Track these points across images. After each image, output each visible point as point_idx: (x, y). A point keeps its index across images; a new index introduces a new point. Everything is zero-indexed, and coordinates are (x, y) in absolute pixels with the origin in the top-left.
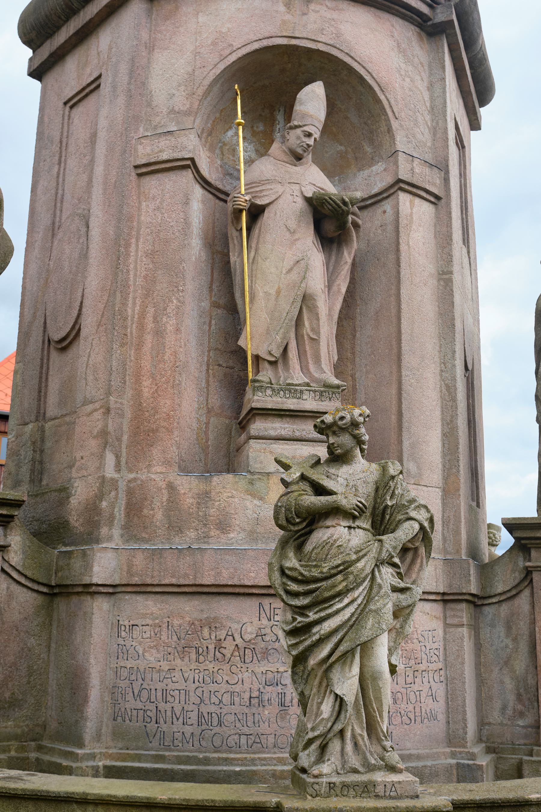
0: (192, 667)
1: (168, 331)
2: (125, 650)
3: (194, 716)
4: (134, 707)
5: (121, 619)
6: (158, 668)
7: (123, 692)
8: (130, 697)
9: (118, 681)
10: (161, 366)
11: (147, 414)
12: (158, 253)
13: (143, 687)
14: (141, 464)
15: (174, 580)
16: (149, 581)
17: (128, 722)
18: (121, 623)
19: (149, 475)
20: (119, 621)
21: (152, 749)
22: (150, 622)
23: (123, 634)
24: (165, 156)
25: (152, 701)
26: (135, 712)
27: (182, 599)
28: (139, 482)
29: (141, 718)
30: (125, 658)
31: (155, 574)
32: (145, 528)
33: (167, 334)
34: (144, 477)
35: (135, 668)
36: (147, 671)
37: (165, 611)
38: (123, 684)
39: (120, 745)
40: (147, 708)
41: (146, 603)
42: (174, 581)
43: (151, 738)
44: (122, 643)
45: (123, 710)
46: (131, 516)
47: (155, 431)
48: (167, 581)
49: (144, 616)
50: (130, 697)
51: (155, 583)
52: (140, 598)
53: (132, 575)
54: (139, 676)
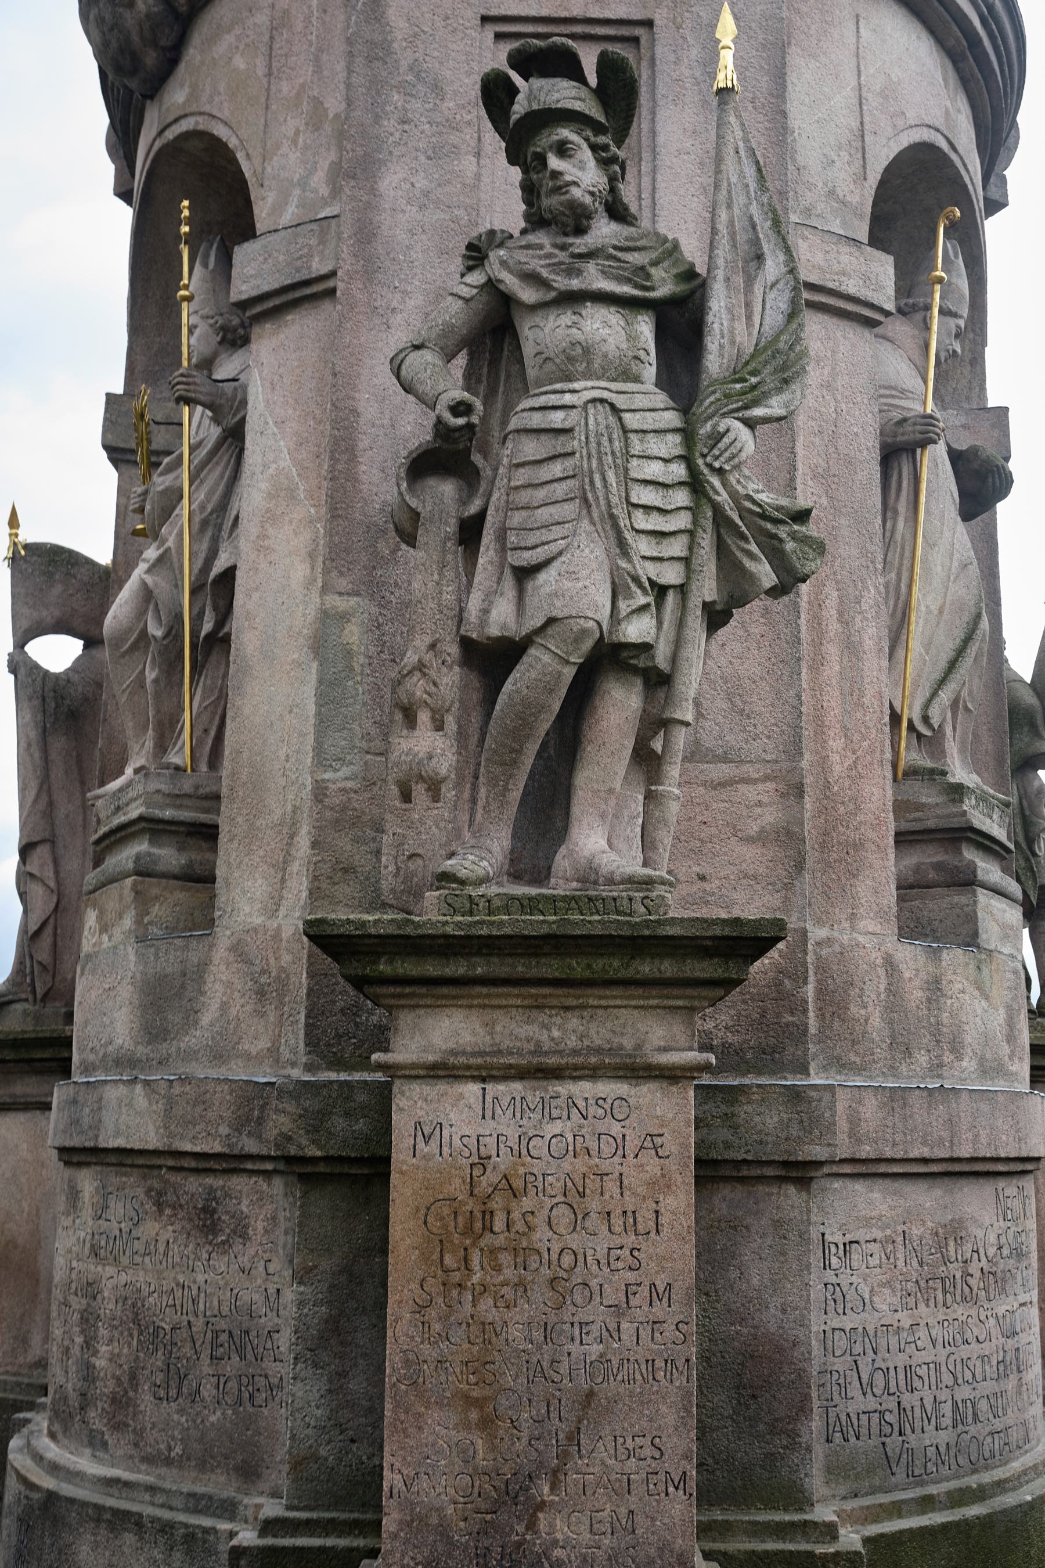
0: (941, 1317)
1: (866, 648)
2: (838, 1295)
3: (947, 1409)
4: (863, 1408)
5: (827, 1232)
6: (896, 1324)
7: (842, 1381)
8: (854, 1390)
9: (831, 1359)
10: (859, 715)
11: (842, 810)
12: (836, 480)
13: (876, 1365)
14: (837, 911)
15: (926, 1149)
16: (888, 1153)
17: (853, 1439)
18: (828, 1238)
19: (855, 935)
20: (823, 1235)
21: (896, 1488)
22: (878, 1234)
23: (834, 1261)
24: (851, 287)
25: (892, 1391)
26: (864, 1418)
27: (922, 1185)
28: (837, 948)
29: (875, 1430)
30: (841, 1311)
31: (898, 1138)
32: (854, 1042)
33: (864, 652)
34: (845, 939)
35: (860, 1329)
36: (879, 1334)
37: (899, 1210)
38: (840, 1364)
39: (842, 1490)
40: (884, 1406)
41: (870, 1195)
42: (926, 1152)
43: (893, 1466)
44: (834, 1280)
45: (843, 1417)
46: (828, 1016)
47: (858, 846)
48: (915, 1153)
49: (867, 1222)
50: (854, 1390)
51: (898, 1156)
52: (859, 1186)
53: (859, 1141)
54: (868, 1346)
